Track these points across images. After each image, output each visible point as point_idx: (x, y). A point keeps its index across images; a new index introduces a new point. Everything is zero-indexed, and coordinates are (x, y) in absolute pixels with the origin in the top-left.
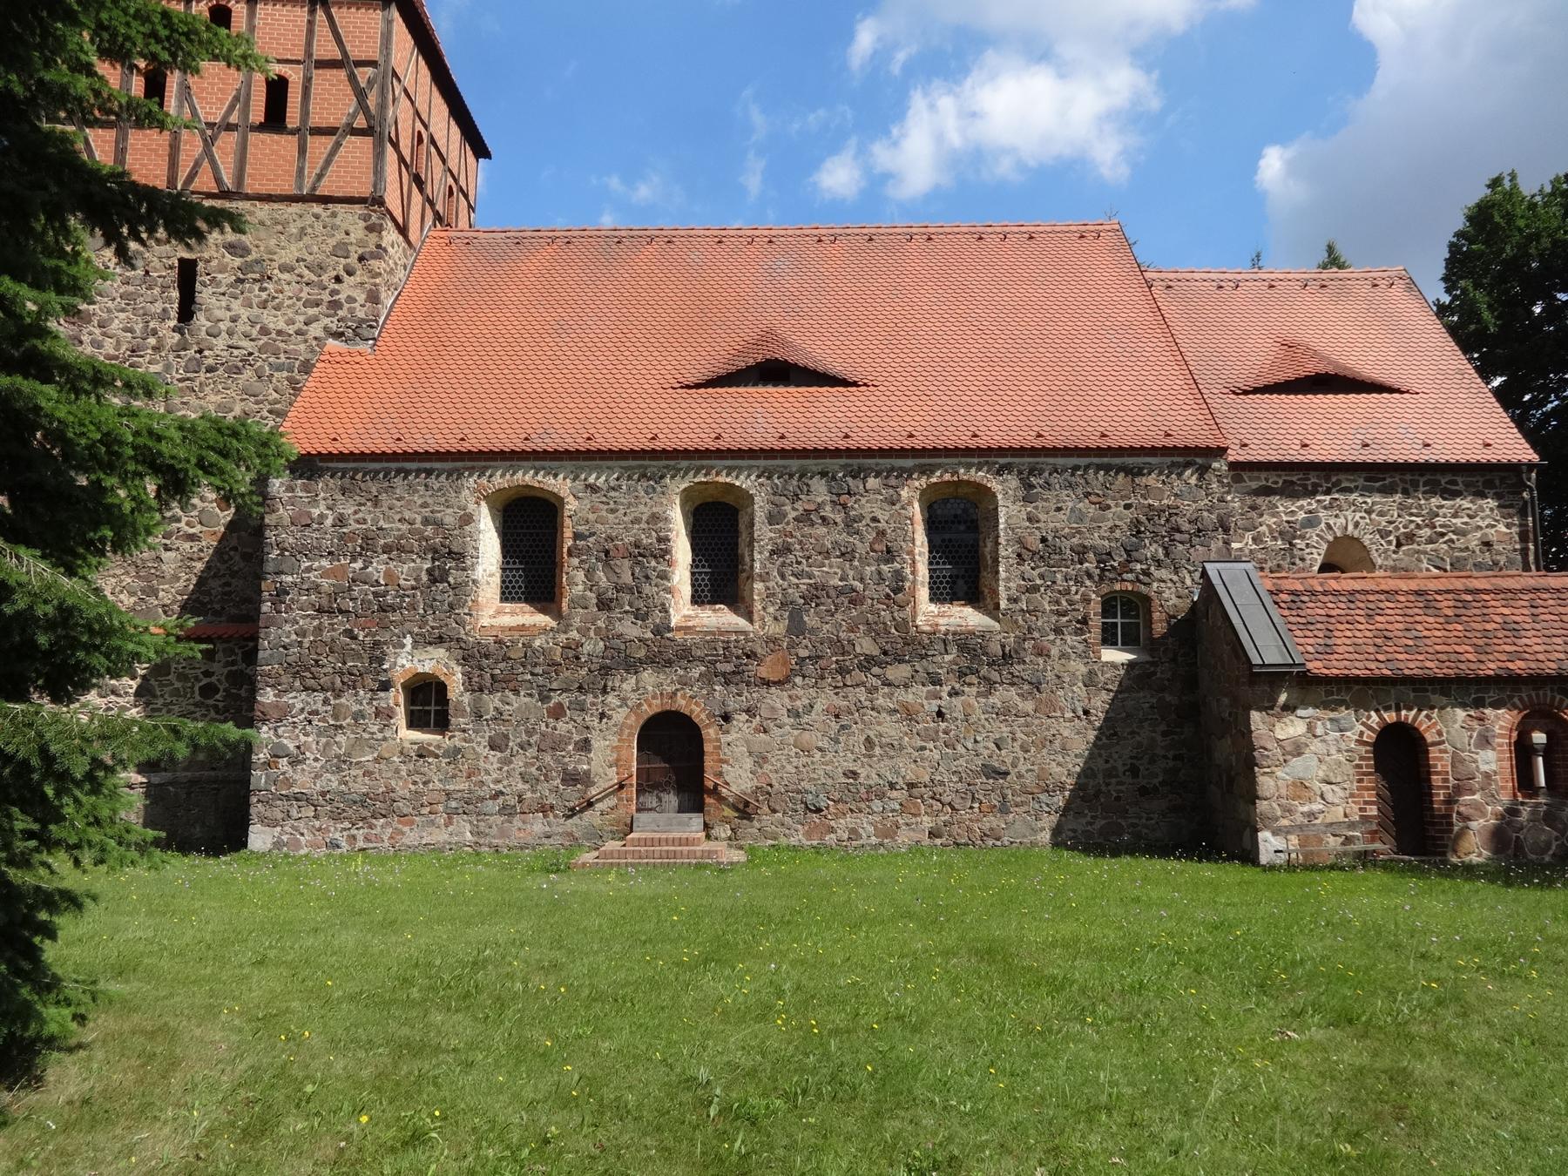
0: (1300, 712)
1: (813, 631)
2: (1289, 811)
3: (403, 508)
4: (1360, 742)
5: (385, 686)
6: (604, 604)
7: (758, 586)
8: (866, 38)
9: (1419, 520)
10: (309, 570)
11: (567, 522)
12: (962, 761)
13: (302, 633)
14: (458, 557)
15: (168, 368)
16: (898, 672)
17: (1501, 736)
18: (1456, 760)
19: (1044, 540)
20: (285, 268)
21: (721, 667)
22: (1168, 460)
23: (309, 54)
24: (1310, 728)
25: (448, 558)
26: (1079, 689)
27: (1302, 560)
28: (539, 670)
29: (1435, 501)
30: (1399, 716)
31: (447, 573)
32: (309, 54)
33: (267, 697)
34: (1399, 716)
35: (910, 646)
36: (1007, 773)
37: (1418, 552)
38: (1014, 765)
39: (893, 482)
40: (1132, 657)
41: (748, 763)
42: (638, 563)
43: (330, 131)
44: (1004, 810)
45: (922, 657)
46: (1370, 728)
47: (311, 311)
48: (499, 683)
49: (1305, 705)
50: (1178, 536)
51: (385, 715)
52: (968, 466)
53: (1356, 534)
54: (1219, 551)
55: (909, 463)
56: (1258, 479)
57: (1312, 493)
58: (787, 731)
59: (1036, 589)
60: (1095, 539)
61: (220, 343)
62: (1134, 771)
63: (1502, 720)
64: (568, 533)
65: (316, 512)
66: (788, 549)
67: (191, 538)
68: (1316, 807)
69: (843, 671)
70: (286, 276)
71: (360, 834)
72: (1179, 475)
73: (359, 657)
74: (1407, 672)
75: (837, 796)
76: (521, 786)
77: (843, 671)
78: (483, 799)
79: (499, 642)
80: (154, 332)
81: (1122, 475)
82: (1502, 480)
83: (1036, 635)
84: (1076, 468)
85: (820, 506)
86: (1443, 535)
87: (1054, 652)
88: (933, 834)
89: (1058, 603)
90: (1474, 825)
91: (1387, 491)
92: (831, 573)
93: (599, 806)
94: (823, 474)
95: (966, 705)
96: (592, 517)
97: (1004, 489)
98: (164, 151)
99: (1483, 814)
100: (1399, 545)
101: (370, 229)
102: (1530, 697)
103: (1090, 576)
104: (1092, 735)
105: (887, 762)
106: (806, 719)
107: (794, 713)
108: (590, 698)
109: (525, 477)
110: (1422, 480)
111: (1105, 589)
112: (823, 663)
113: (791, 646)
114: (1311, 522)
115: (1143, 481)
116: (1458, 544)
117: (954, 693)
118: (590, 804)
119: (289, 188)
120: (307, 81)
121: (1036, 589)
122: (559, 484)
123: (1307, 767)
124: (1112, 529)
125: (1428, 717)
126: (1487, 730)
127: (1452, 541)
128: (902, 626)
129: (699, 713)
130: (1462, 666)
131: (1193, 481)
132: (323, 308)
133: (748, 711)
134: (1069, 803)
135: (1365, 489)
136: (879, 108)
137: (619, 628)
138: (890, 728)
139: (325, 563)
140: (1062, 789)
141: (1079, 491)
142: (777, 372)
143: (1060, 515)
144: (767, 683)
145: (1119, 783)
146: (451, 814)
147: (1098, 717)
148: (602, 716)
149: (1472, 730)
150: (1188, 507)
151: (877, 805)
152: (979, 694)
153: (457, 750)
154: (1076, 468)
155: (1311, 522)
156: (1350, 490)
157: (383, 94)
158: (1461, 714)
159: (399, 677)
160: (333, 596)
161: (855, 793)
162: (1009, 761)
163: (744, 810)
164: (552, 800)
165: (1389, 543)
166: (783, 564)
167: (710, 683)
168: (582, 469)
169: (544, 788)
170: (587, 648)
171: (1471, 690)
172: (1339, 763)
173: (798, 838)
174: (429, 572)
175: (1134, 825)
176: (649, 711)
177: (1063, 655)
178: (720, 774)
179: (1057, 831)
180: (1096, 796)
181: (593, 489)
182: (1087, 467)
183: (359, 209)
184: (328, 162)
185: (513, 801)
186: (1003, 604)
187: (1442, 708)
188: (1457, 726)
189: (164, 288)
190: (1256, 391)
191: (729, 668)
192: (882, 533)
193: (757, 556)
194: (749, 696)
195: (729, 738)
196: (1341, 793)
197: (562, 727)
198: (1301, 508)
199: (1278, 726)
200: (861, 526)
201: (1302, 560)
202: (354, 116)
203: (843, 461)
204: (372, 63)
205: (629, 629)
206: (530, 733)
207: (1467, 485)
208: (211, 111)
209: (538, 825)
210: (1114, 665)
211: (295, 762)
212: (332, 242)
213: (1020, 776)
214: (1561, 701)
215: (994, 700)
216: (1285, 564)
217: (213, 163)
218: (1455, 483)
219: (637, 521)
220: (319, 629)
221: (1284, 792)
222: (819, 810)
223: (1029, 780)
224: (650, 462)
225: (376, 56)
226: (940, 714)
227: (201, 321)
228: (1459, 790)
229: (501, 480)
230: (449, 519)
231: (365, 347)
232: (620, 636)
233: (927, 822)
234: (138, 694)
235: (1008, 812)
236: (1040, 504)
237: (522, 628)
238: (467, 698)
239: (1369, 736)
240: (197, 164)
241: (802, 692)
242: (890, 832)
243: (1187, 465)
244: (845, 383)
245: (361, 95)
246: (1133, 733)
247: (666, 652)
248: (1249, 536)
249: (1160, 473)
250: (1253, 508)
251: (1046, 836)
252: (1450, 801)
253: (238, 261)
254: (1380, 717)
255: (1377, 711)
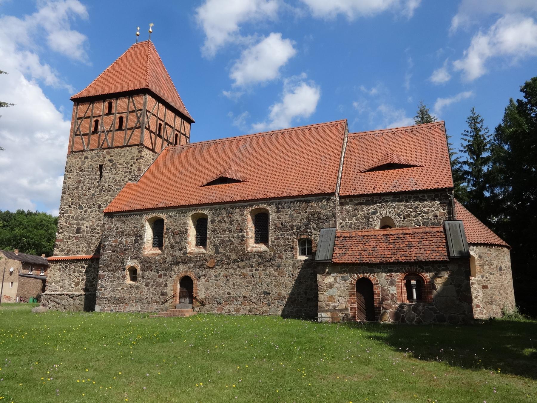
0: (332, 275)
1: (221, 253)
2: (328, 305)
3: (129, 225)
4: (351, 284)
5: (124, 270)
6: (172, 247)
7: (208, 241)
8: (456, 21)
9: (411, 210)
10: (110, 241)
11: (165, 226)
12: (258, 290)
13: (108, 257)
14: (141, 236)
15: (96, 192)
16: (242, 264)
17: (398, 282)
18: (383, 290)
19: (282, 224)
20: (121, 164)
21: (199, 263)
22: (318, 197)
23: (128, 110)
24: (335, 280)
25: (139, 236)
26: (291, 268)
27: (372, 225)
28: (157, 265)
29: (417, 203)
30: (364, 275)
31: (138, 240)
32: (128, 110)
33: (101, 273)
34: (364, 275)
35: (245, 256)
36: (270, 294)
37: (411, 220)
38: (272, 291)
39: (242, 209)
40: (307, 258)
41: (204, 290)
42: (180, 236)
43: (131, 129)
44: (269, 304)
45: (249, 259)
46: (354, 279)
47: (126, 174)
48: (149, 269)
49: (334, 272)
50: (320, 220)
51: (124, 277)
52: (262, 204)
53: (390, 216)
54: (332, 224)
55: (246, 204)
56: (358, 200)
57: (375, 203)
58: (213, 281)
59: (279, 238)
60: (297, 223)
61: (106, 184)
62: (306, 293)
63: (398, 276)
64: (165, 229)
65: (112, 226)
66: (215, 230)
67: (98, 233)
68: (336, 304)
69: (228, 264)
70: (121, 166)
71: (117, 308)
72: (321, 202)
73: (119, 263)
74: (430, 260)
75: (225, 300)
76: (152, 296)
77: (228, 264)
78: (143, 299)
79: (148, 258)
80: (93, 183)
81: (304, 203)
82: (441, 194)
83: (279, 252)
84: (291, 202)
85: (224, 218)
86: (420, 214)
87: (284, 257)
88: (250, 311)
89: (285, 242)
90: (388, 311)
91: (400, 201)
92: (226, 236)
93: (169, 302)
94: (225, 209)
95: (260, 273)
96: (170, 224)
97: (271, 209)
98: (97, 139)
99: (391, 308)
100: (404, 218)
101: (139, 152)
102: (408, 269)
103: (295, 234)
104: (294, 282)
105: (238, 290)
106: (218, 278)
107: (215, 276)
108: (168, 272)
109: (156, 214)
110: (412, 196)
111: (299, 238)
112: (223, 262)
113: (215, 257)
114: (375, 213)
115: (310, 204)
116: (425, 217)
117: (256, 270)
118: (167, 301)
119: (122, 144)
120: (127, 116)
121: (279, 238)
122: (163, 216)
123: (334, 292)
124: (301, 220)
125: (373, 276)
126: (393, 280)
127: (423, 216)
128: (243, 251)
129: (192, 276)
130: (383, 259)
131: (325, 203)
132: (128, 173)
133: (204, 275)
134: (287, 302)
135: (392, 201)
136: (461, 44)
137: (175, 253)
138: (239, 280)
139: (113, 239)
140: (285, 298)
141: (292, 209)
142: (223, 180)
143: (287, 216)
144: (209, 268)
145: (301, 297)
146: (137, 303)
147: (296, 276)
148: (170, 277)
149: (388, 280)
150: (323, 211)
151: (235, 302)
152: (263, 270)
153: (138, 286)
154: (291, 202)
155: (375, 213)
156: (387, 202)
157: (144, 117)
158: (384, 275)
159: (127, 267)
160: (115, 247)
161: (230, 299)
162: (270, 290)
163: (202, 304)
164: (158, 300)
165: (401, 218)
166: (214, 234)
167: (196, 268)
168: (168, 211)
169: (157, 296)
170: (168, 259)
171: (388, 267)
172: (344, 291)
173: (215, 312)
174: (135, 240)
175: (305, 310)
176: (181, 275)
177: (287, 258)
178: (197, 293)
179: (283, 311)
180: (295, 301)
181: (171, 216)
182: (294, 201)
183: (137, 147)
184: (131, 136)
185: (150, 300)
186: (270, 243)
187: (378, 273)
188: (383, 279)
189: (96, 172)
190: (368, 171)
191: (200, 264)
192: (239, 224)
193: (208, 232)
194: (205, 271)
195: (199, 283)
196: (345, 300)
197: (162, 280)
198: (371, 208)
199: (326, 279)
200: (234, 223)
201: (372, 225)
202: (136, 124)
203: (230, 205)
204: (141, 110)
205: (178, 254)
206: (154, 282)
207: (428, 197)
208: (107, 128)
209: (155, 306)
210: (301, 261)
211: (105, 289)
212: (131, 156)
213: (273, 294)
214: (419, 270)
215: (267, 272)
216: (366, 227)
217: (107, 140)
218: (424, 196)
219: (180, 224)
220: (111, 256)
221: (326, 299)
222: (220, 304)
223: (276, 295)
224: (183, 209)
225: (142, 108)
226: (253, 276)
227: (103, 179)
228: (383, 300)
229: (151, 216)
230: (139, 226)
231: (135, 182)
232: (175, 256)
233: (248, 308)
234: (85, 272)
235: (270, 305)
236: (281, 213)
237: (153, 254)
238: (141, 273)
239: (354, 282)
240: (104, 141)
241: (218, 270)
242: (237, 311)
243: (323, 199)
244: (240, 181)
245: (138, 118)
246: (306, 281)
247: (186, 260)
248: (354, 218)
249: (316, 202)
250: (356, 209)
251: (280, 313)
252: (380, 303)
253: (111, 164)
254: (358, 276)
255: (357, 274)
